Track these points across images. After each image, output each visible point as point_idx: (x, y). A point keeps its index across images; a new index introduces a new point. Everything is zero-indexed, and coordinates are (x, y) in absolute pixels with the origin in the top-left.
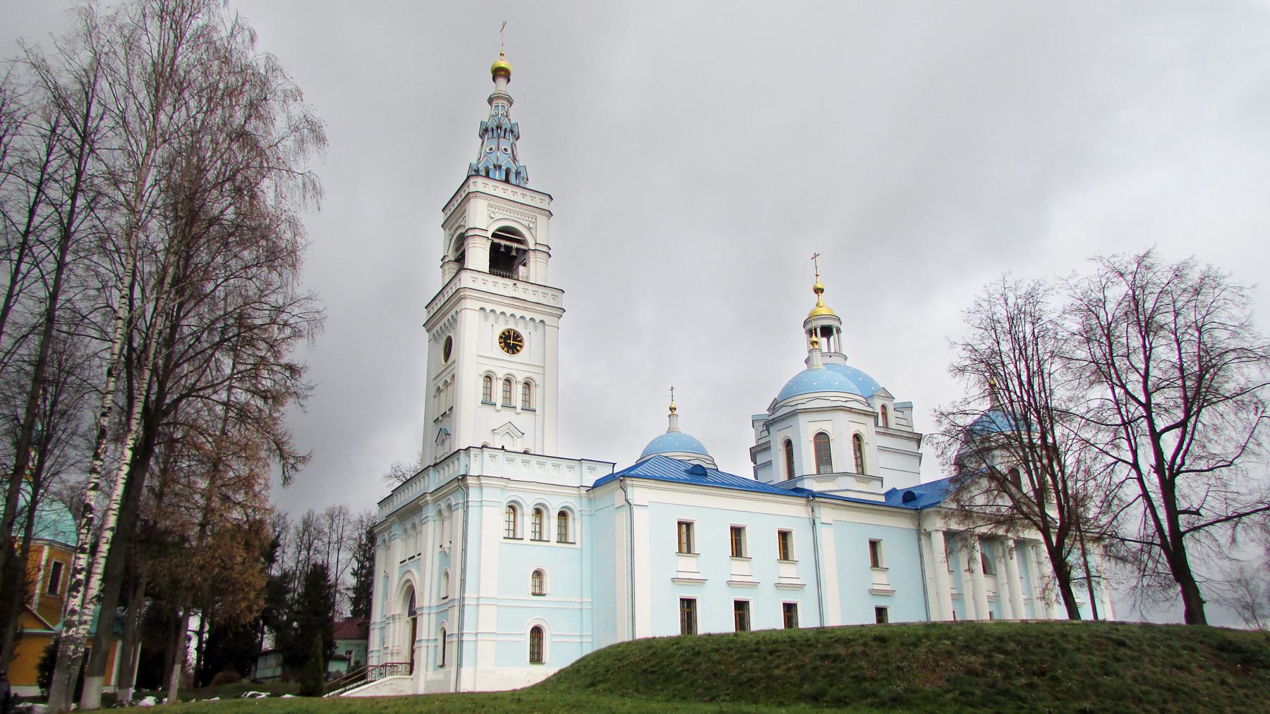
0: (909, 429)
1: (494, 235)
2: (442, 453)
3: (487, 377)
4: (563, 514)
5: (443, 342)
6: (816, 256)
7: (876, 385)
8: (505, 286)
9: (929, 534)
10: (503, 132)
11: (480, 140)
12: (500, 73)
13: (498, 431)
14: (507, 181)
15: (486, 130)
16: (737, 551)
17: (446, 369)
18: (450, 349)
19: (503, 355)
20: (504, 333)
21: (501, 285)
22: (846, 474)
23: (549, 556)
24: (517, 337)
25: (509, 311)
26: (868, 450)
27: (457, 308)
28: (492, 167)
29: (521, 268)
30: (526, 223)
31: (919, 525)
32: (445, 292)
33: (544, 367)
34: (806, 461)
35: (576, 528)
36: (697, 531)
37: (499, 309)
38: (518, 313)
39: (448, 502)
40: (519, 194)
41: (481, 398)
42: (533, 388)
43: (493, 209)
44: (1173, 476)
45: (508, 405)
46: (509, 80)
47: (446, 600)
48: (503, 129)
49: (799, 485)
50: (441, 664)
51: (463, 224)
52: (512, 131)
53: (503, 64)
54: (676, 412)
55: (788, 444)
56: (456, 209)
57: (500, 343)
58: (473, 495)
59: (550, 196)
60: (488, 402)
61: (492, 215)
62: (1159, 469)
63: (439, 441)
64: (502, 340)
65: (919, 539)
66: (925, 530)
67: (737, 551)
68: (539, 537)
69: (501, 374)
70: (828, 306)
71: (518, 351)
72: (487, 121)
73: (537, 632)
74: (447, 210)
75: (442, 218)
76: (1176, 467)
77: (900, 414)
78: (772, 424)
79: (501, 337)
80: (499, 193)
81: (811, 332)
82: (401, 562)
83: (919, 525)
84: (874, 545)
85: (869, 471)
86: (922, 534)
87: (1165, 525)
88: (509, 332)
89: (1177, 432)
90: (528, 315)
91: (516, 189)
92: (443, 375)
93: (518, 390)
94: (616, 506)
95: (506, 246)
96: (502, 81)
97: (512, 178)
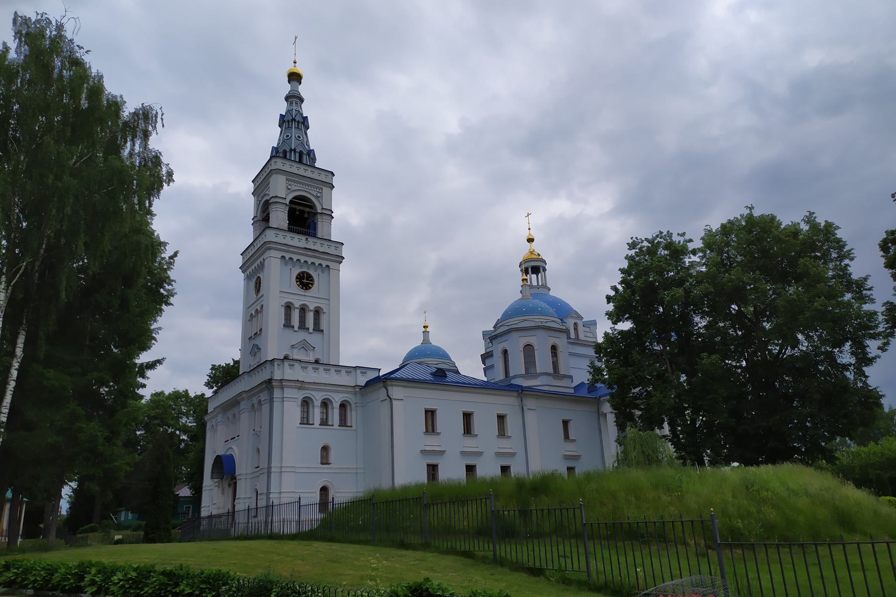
1: (291, 202)
4: (343, 406)
5: (254, 280)
6: (528, 215)
8: (300, 240)
9: (605, 415)
13: (296, 346)
14: (300, 161)
17: (256, 301)
21: (298, 241)
23: (333, 435)
24: (309, 277)
25: (303, 259)
27: (265, 256)
30: (315, 193)
31: (598, 409)
33: (329, 300)
35: (353, 417)
36: (439, 417)
37: (295, 257)
38: (310, 260)
41: (283, 322)
43: (290, 183)
45: (303, 326)
47: (258, 469)
51: (267, 193)
54: (428, 330)
55: (505, 352)
57: (297, 282)
58: (277, 393)
59: (332, 172)
60: (288, 325)
61: (289, 187)
64: (298, 280)
71: (310, 288)
77: (588, 330)
78: (494, 339)
79: (297, 278)
81: (526, 271)
83: (598, 409)
84: (565, 423)
85: (562, 371)
90: (317, 262)
93: (310, 317)
95: (300, 210)
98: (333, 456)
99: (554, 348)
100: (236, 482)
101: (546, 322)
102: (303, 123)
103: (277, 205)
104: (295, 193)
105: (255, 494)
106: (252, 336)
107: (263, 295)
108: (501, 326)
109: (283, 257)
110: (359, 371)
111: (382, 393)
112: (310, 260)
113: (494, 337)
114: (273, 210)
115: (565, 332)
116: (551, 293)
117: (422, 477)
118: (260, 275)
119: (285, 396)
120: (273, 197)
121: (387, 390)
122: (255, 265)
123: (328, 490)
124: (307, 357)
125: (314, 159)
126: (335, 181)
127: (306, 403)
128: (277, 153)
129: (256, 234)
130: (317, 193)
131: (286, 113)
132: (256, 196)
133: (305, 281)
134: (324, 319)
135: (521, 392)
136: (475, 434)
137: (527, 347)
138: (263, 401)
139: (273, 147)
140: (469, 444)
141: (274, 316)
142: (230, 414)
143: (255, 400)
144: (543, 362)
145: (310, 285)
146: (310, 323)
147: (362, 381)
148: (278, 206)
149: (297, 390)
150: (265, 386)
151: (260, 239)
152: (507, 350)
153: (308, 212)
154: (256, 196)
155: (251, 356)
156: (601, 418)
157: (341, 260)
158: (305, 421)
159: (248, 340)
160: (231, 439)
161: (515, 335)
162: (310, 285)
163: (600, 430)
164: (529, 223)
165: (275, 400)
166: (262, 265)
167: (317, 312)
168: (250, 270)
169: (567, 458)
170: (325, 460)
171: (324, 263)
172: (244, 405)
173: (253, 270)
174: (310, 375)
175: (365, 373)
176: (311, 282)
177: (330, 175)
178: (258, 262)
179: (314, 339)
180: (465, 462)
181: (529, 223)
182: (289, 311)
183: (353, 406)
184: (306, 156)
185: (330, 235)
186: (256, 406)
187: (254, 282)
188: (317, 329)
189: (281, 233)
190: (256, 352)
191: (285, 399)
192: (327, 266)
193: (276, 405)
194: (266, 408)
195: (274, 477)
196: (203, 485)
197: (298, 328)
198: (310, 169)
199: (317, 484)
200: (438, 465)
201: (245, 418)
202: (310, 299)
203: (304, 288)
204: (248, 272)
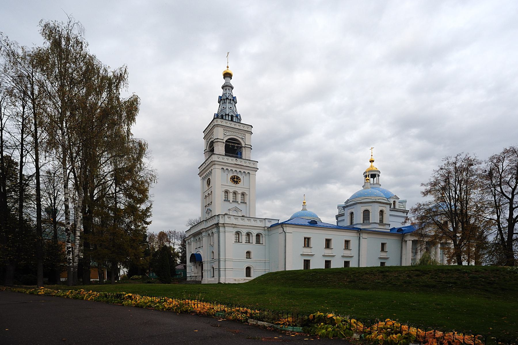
1: (226, 141)
2: (208, 217)
4: (258, 235)
8: (232, 160)
14: (232, 120)
17: (208, 189)
19: (233, 184)
20: (232, 177)
21: (231, 160)
23: (253, 247)
24: (238, 178)
25: (234, 169)
26: (385, 216)
27: (212, 168)
30: (241, 137)
31: (402, 239)
33: (249, 189)
40: (228, 123)
41: (224, 199)
43: (226, 131)
46: (231, 79)
47: (213, 259)
55: (352, 214)
57: (231, 180)
58: (221, 229)
59: (251, 126)
61: (225, 134)
78: (346, 207)
79: (231, 178)
85: (384, 222)
90: (242, 171)
92: (208, 191)
97: (234, 120)
98: (252, 255)
107: (212, 187)
114: (216, 145)
122: (207, 172)
125: (240, 119)
127: (238, 233)
128: (217, 117)
131: (222, 95)
132: (206, 140)
133: (236, 180)
135: (359, 231)
142: (197, 238)
145: (238, 182)
147: (269, 225)
151: (209, 160)
154: (206, 140)
158: (238, 241)
160: (199, 248)
162: (238, 182)
164: (372, 153)
166: (211, 172)
167: (243, 194)
172: (204, 234)
174: (240, 222)
177: (250, 127)
178: (208, 171)
179: (241, 207)
183: (263, 235)
184: (235, 118)
185: (250, 157)
186: (210, 234)
188: (244, 203)
191: (226, 232)
194: (216, 235)
201: (205, 240)
202: (239, 188)
203: (235, 183)
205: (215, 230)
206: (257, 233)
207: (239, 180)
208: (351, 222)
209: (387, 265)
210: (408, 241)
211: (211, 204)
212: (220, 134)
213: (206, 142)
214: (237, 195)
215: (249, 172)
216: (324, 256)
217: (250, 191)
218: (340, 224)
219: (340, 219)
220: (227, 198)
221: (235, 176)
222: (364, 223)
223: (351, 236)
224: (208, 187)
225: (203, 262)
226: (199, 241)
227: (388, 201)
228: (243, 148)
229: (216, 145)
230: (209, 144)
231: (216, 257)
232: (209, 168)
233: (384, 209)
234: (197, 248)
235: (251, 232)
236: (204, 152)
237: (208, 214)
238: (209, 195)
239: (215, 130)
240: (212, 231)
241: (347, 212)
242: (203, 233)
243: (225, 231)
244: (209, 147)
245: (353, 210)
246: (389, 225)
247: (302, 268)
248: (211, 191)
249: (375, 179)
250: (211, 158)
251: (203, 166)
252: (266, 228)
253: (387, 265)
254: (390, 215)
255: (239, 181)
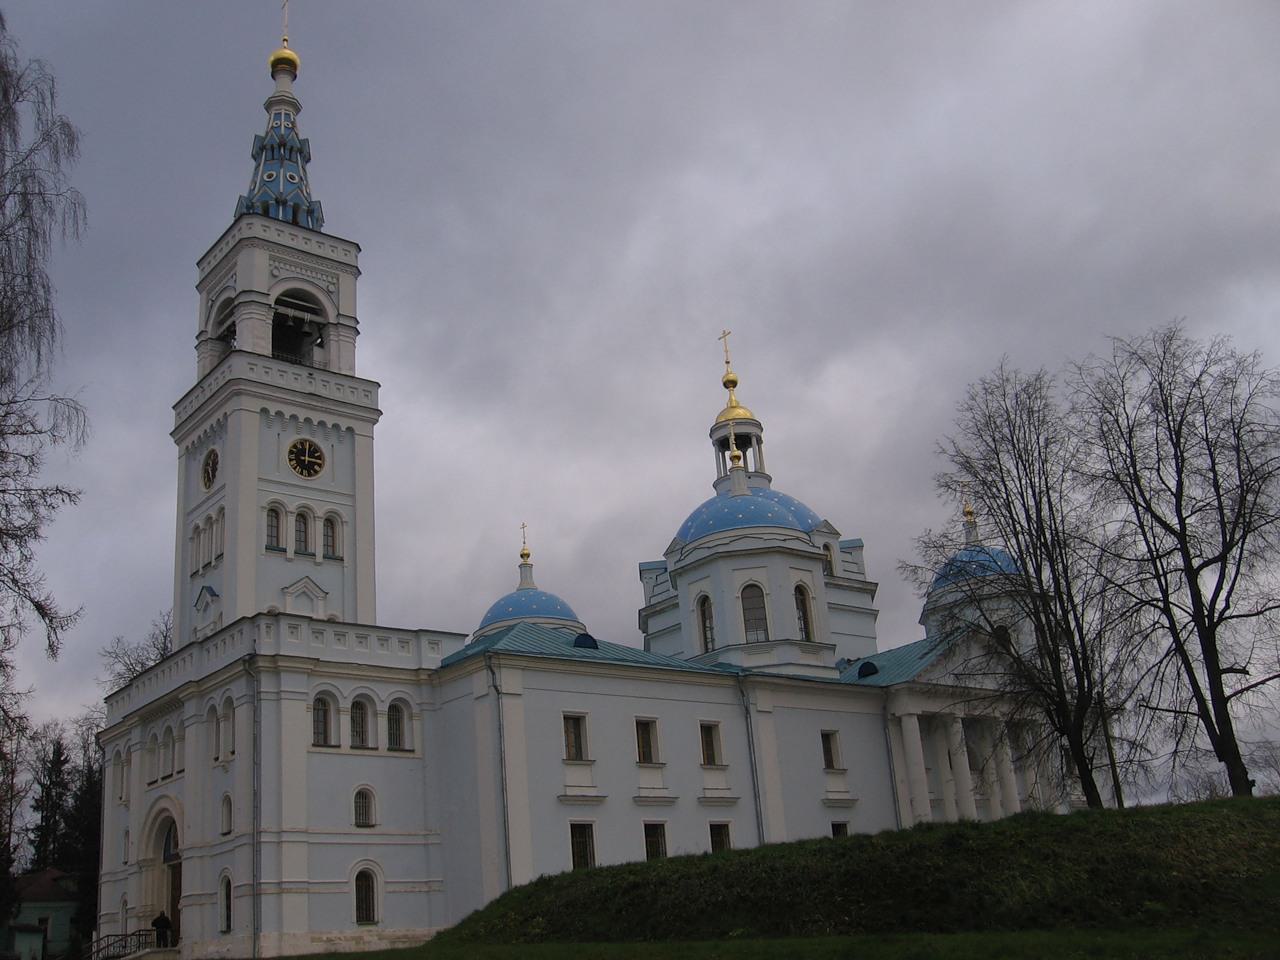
0: (860, 577)
1: (278, 302)
2: (205, 626)
3: (272, 510)
4: (395, 712)
5: (202, 458)
6: (725, 334)
7: (814, 517)
8: (297, 377)
9: (899, 721)
10: (287, 152)
11: (253, 163)
12: (283, 67)
13: (290, 590)
14: (295, 223)
15: (262, 148)
16: (646, 756)
17: (208, 499)
18: (214, 470)
19: (295, 477)
20: (295, 446)
21: (289, 377)
22: (788, 642)
23: (374, 770)
24: (315, 451)
25: (302, 414)
26: (817, 609)
27: (228, 408)
28: (273, 202)
29: (317, 351)
30: (323, 285)
31: (885, 708)
32: (205, 385)
33: (353, 496)
34: (730, 624)
35: (414, 732)
36: (590, 728)
37: (288, 411)
38: (316, 417)
39: (228, 694)
40: (273, 229)
41: (264, 541)
42: (338, 528)
43: (277, 264)
44: (1214, 626)
45: (303, 551)
46: (295, 77)
47: (229, 837)
48: (288, 147)
49: (721, 660)
50: (224, 929)
51: (231, 283)
52: (301, 152)
53: (288, 53)
54: (530, 561)
55: (704, 601)
56: (217, 266)
57: (291, 460)
58: (266, 684)
59: (357, 245)
60: (274, 547)
61: (276, 272)
62: (1197, 616)
63: (201, 606)
64: (293, 457)
65: (885, 728)
66: (894, 714)
67: (646, 756)
68: (360, 741)
69: (293, 506)
70: (747, 405)
71: (316, 472)
72: (263, 134)
73: (365, 881)
74: (205, 264)
75: (196, 276)
76: (1216, 615)
77: (848, 557)
78: (680, 575)
79: (291, 452)
80: (285, 240)
81: (722, 445)
82: (150, 784)
83: (885, 708)
84: (827, 737)
85: (818, 636)
86: (889, 721)
87: (1207, 695)
88: (302, 444)
89: (1216, 567)
90: (330, 421)
91: (308, 235)
92: (204, 508)
93: (317, 529)
94: (475, 696)
95: (295, 318)
96: (284, 79)
97: (302, 218)
98: (378, 811)
99: (800, 591)
100: (181, 864)
101: (785, 540)
102: (301, 152)
103: (253, 307)
104: (284, 284)
105: (224, 887)
106: (198, 571)
107: (224, 486)
108: (695, 548)
109: (264, 411)
110: (424, 640)
111: (480, 682)
112: (316, 417)
113: (680, 571)
114: (244, 317)
115: (820, 559)
116: (773, 486)
117: (638, 853)
118: (217, 448)
119: (283, 689)
120: (244, 292)
121: (493, 673)
122: (206, 426)
123: (372, 878)
124: (313, 611)
125: (320, 221)
126: (362, 262)
127: (322, 706)
128: (248, 209)
129: (204, 366)
130: (327, 284)
131: (267, 133)
132: (205, 293)
133: (307, 458)
134: (343, 533)
135: (743, 681)
136: (661, 762)
137: (746, 591)
138: (237, 699)
139: (241, 196)
140: (650, 781)
141: (247, 528)
142: (158, 728)
143: (218, 700)
144: (782, 618)
145: (316, 467)
146: (317, 544)
147: (432, 659)
148: (253, 308)
149: (520, 672)
150: (241, 668)
151: (217, 374)
152: (707, 597)
153: (311, 322)
154: (205, 293)
155: (198, 610)
156: (892, 729)
157: (375, 417)
158: (322, 738)
159: (189, 578)
160: (163, 779)
161: (724, 568)
162: (316, 467)
163: (889, 752)
164: (727, 351)
165: (263, 696)
166: (222, 425)
167: (330, 522)
168: (194, 437)
169: (831, 804)
170: (363, 819)
171: (344, 424)
172: (190, 708)
173: (200, 437)
174: (331, 649)
175: (387, 640)
176: (318, 461)
177: (353, 250)
178: (213, 421)
179: (326, 575)
180: (708, 820)
181: (727, 351)
182: (274, 519)
183: (415, 710)
184: (303, 215)
185: (353, 368)
186: (220, 710)
187: (202, 462)
188: (332, 556)
189: (260, 362)
190: (207, 603)
191: (283, 695)
192: (350, 429)
193: (267, 708)
194: (242, 713)
195: (267, 852)
196: (102, 873)
197: (295, 553)
198: (315, 238)
199: (350, 867)
200: (663, 825)
201: (195, 740)
202: (316, 495)
203: (305, 472)
204: (188, 442)
205: (238, 690)
206: (355, 695)
207: (319, 458)
208: (706, 641)
209: (851, 831)
210: (904, 719)
211: (215, 567)
212: (258, 273)
213: (204, 302)
214: (282, 517)
215: (294, 412)
216: (563, 799)
217: (354, 506)
218: (663, 649)
219: (655, 625)
220: (333, 546)
221: (306, 441)
222: (748, 647)
223: (715, 704)
224: (205, 490)
225: (185, 855)
226: (166, 745)
227: (814, 546)
228: (332, 331)
229: (244, 317)
230: (215, 309)
231: (242, 824)
232: (216, 410)
233: (806, 579)
234: (156, 781)
235: (334, 691)
236: (197, 343)
237: (201, 612)
238: (212, 525)
239: (243, 258)
240: (226, 695)
241: (689, 593)
242: (186, 705)
243: (278, 693)
244: (214, 322)
245: (705, 587)
246: (833, 647)
247: (568, 866)
248: (217, 507)
249: (750, 452)
250: (227, 365)
251: (192, 397)
252: (423, 677)
253: (851, 831)
254: (832, 607)
255: (320, 465)
